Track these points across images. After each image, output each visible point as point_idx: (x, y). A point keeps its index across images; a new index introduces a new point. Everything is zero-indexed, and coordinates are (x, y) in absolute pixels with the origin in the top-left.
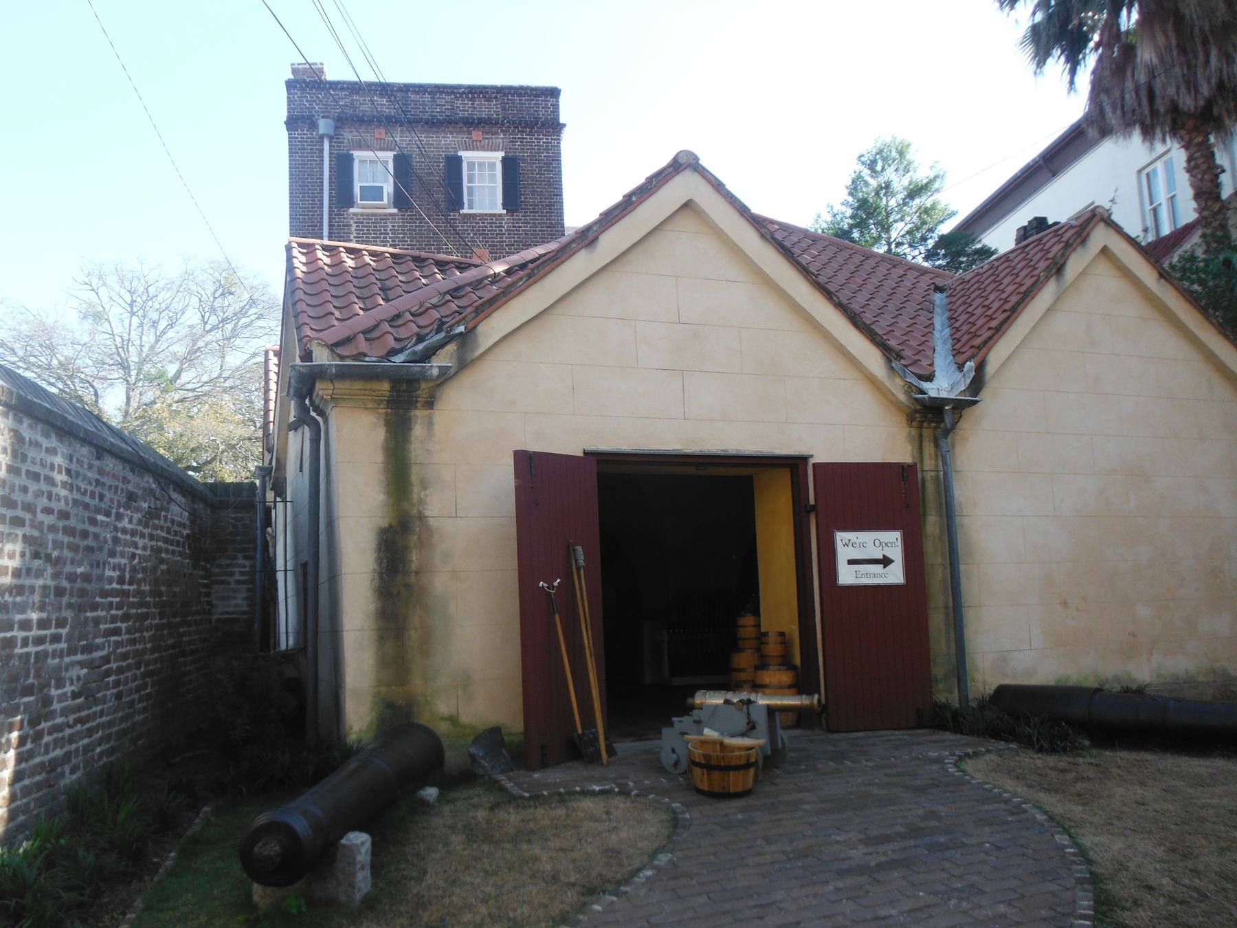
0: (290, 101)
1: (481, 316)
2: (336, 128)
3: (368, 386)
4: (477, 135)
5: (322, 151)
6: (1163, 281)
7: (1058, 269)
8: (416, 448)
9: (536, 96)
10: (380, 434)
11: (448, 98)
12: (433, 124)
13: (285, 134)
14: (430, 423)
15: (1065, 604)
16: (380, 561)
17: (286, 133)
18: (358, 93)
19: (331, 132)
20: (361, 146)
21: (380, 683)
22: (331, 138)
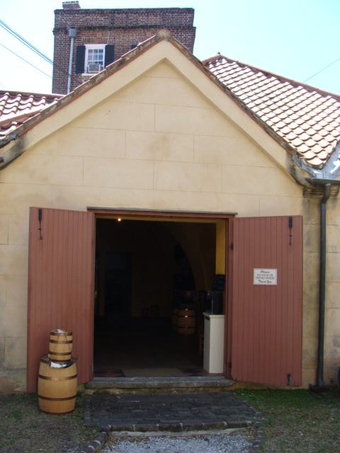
0: (56, 21)
5: (70, 45)
12: (126, 29)
13: (52, 37)
20: (90, 42)
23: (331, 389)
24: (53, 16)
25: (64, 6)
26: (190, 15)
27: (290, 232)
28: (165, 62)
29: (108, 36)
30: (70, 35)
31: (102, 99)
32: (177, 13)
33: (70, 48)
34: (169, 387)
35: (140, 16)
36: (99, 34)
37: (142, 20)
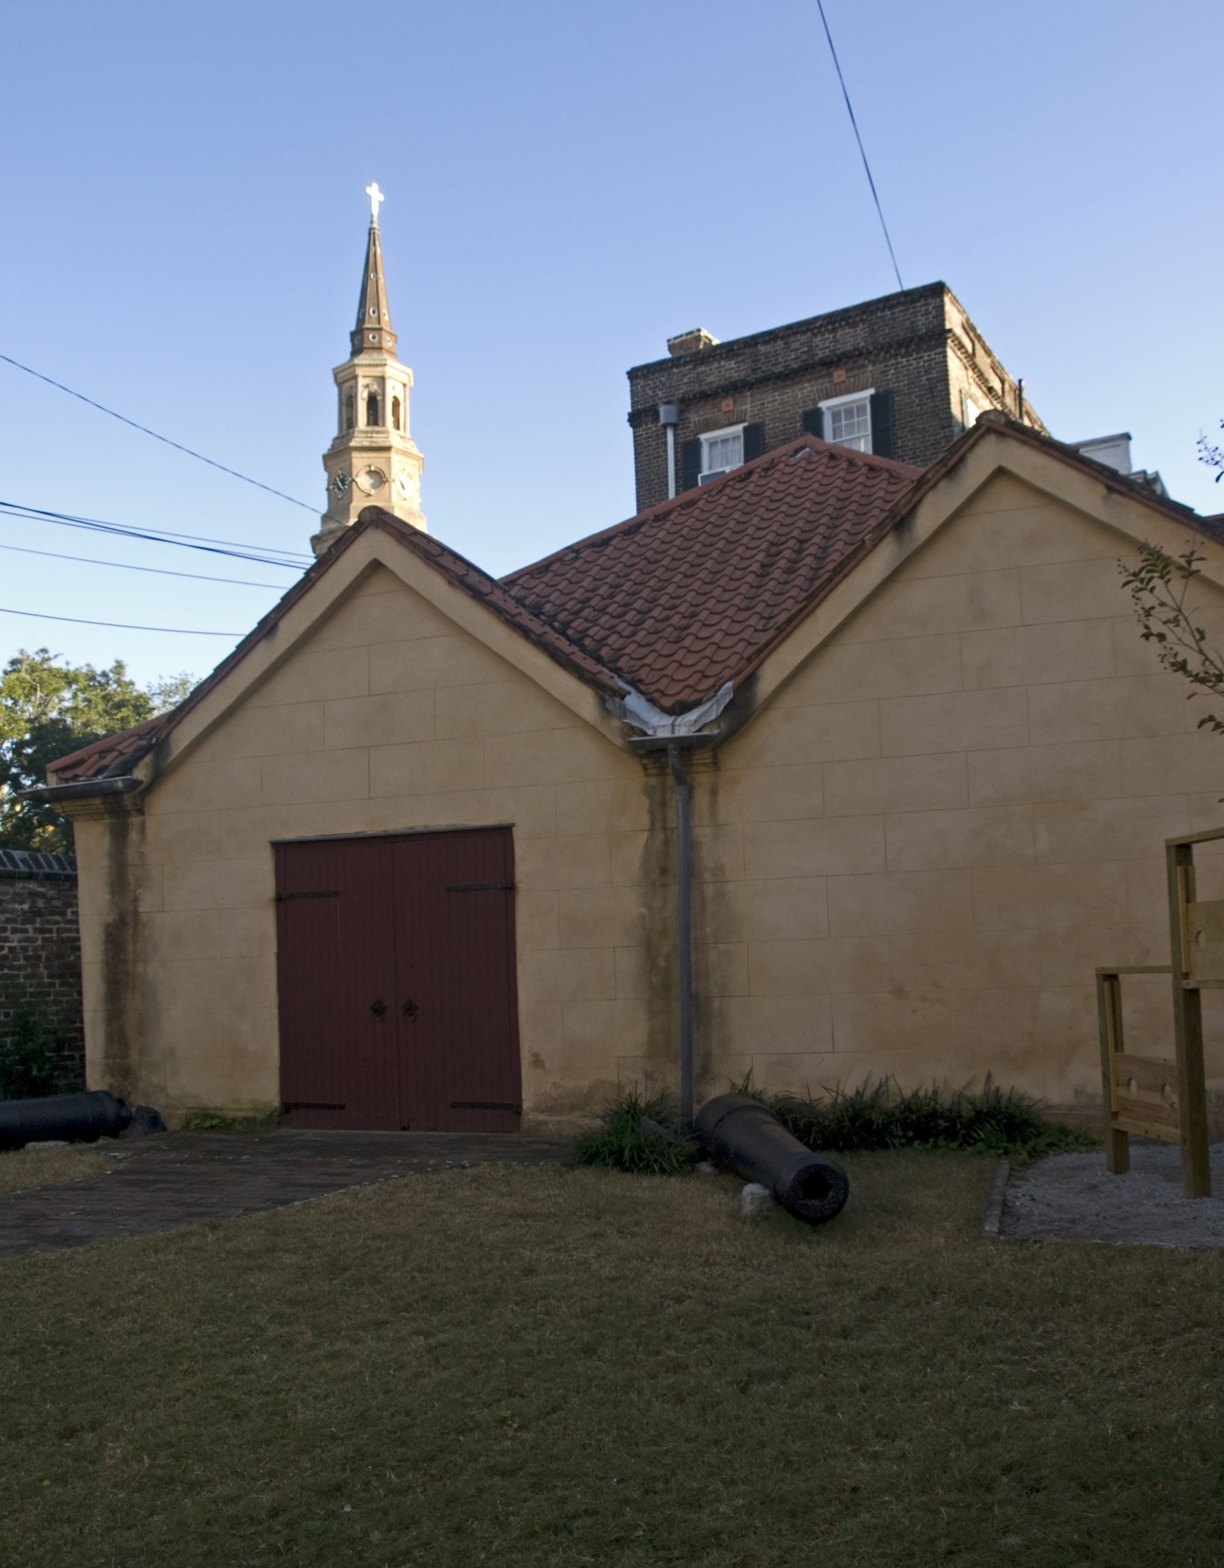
0: (634, 394)
1: (174, 723)
2: (681, 412)
3: (85, 802)
4: (839, 375)
5: (665, 443)
6: (1116, 497)
7: (901, 522)
8: (131, 854)
9: (913, 302)
10: (106, 842)
11: (804, 338)
12: (787, 377)
13: (629, 432)
14: (142, 829)
15: (899, 992)
16: (106, 951)
17: (631, 430)
18: (702, 363)
19: (673, 419)
20: (708, 427)
21: (107, 1056)
22: (675, 426)
23: (238, 1126)
24: (626, 384)
25: (671, 348)
26: (933, 302)
27: (678, 872)
28: (376, 567)
29: (748, 405)
30: (662, 420)
31: (1048, 488)
32: (903, 304)
33: (666, 451)
34: (547, 1123)
35: (815, 335)
36: (727, 404)
37: (824, 345)
